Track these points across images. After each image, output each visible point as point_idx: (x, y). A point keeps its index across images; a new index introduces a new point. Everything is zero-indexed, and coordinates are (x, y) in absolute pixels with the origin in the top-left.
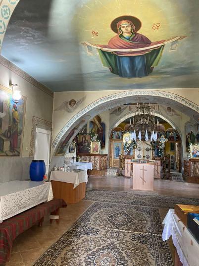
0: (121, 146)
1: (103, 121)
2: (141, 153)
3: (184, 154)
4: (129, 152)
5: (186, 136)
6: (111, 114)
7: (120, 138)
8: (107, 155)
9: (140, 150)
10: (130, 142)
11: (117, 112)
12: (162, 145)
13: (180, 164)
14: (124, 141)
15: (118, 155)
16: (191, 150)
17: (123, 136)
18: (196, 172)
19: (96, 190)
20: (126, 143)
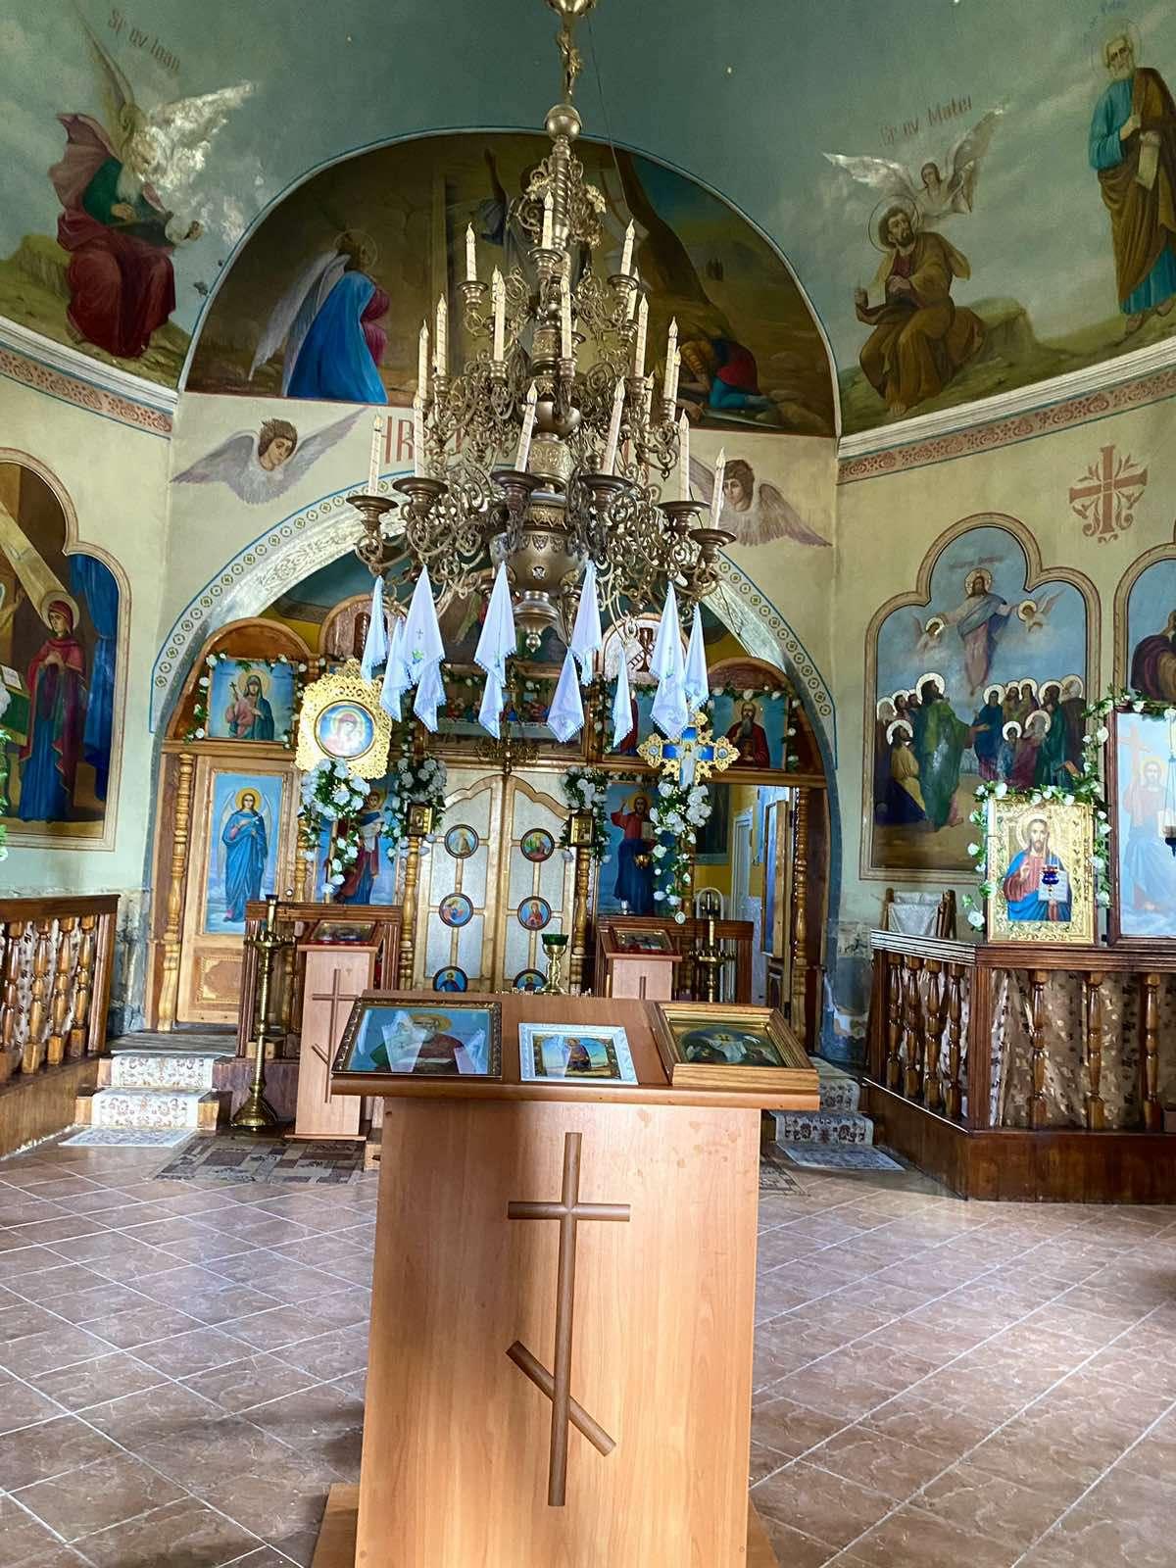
0: (283, 814)
1: (86, 534)
2: (477, 880)
3: (859, 892)
4: (359, 873)
5: (880, 728)
6: (183, 477)
7: (267, 731)
8: (106, 904)
9: (467, 852)
10: (372, 764)
11: (254, 466)
12: (682, 799)
13: (811, 979)
14: (309, 758)
15: (246, 902)
16: (993, 845)
17: (297, 706)
18: (1035, 1083)
19: (1144, 263)
20: (329, 782)
